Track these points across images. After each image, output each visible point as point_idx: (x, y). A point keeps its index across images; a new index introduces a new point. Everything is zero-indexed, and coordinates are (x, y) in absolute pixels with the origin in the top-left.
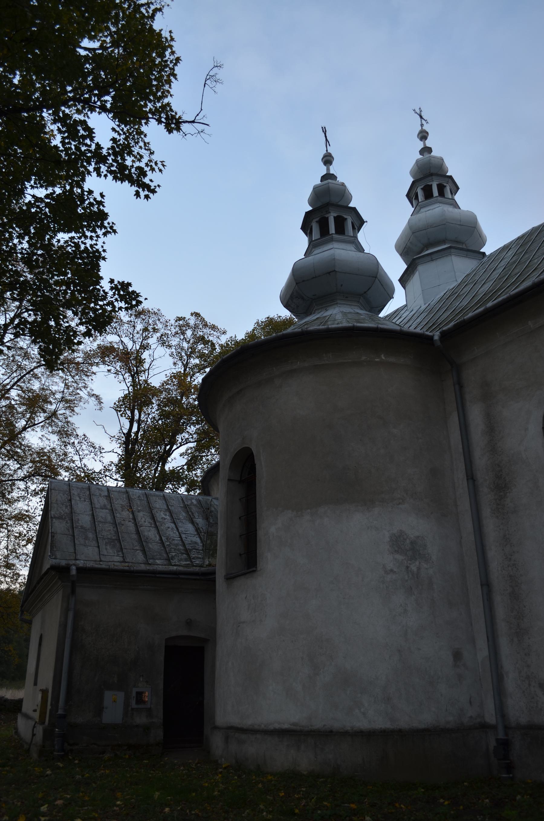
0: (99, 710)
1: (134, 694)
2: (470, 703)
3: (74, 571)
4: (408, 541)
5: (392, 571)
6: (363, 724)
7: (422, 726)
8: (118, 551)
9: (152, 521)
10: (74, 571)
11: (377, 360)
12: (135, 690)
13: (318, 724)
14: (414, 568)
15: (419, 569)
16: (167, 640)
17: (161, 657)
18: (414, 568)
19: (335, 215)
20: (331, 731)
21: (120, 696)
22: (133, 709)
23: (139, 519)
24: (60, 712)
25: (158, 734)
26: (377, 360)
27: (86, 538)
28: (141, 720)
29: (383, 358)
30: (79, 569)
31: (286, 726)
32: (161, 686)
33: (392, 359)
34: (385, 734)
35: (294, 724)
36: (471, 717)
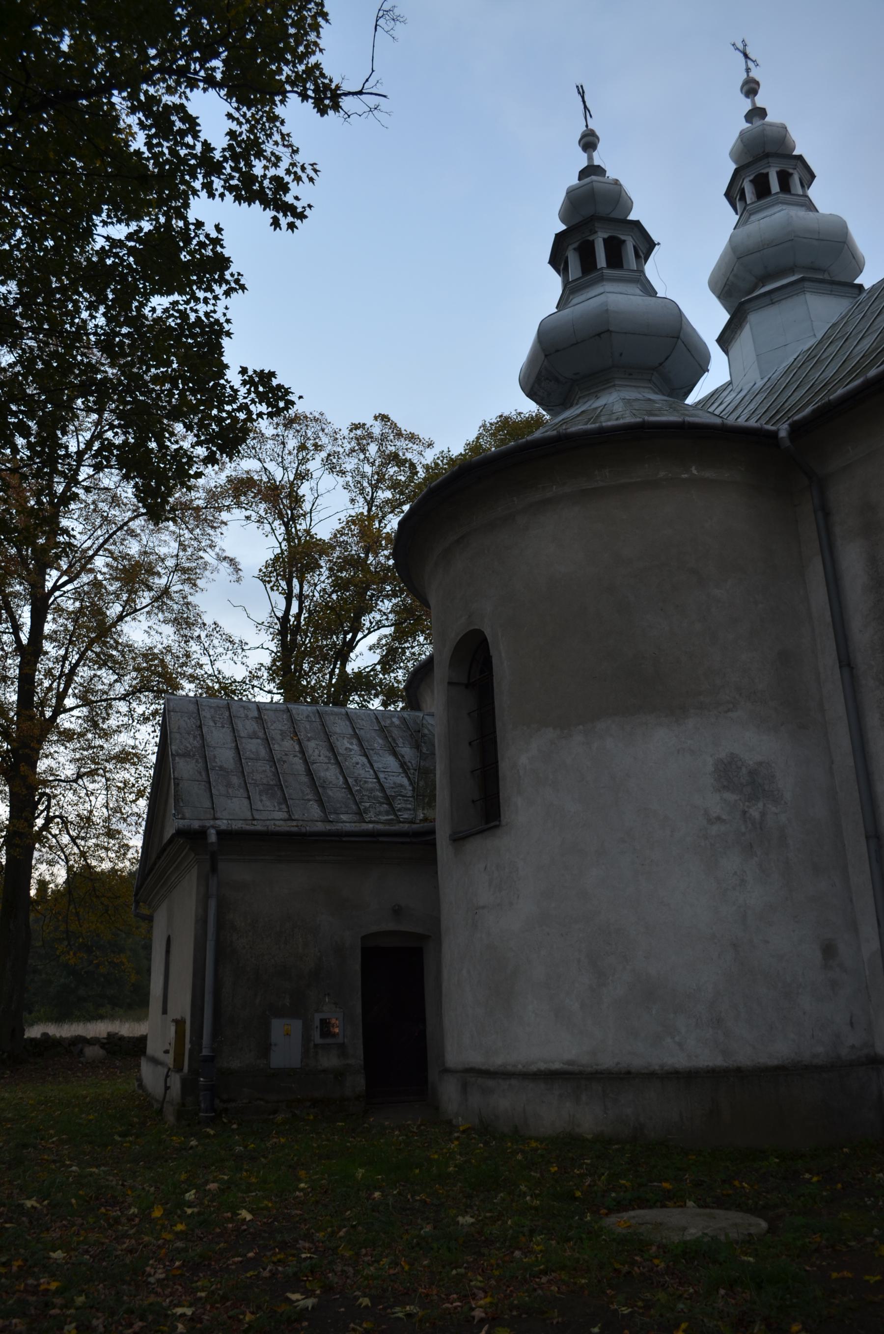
0: (265, 1048)
1: (317, 1023)
2: (852, 1024)
3: (213, 837)
4: (744, 770)
5: (718, 818)
6: (679, 1060)
7: (775, 1062)
8: (280, 804)
9: (330, 755)
10: (213, 837)
11: (685, 476)
12: (317, 1017)
13: (607, 1062)
14: (755, 813)
15: (763, 814)
16: (364, 938)
17: (355, 965)
18: (755, 813)
19: (606, 236)
20: (629, 1073)
21: (296, 1026)
22: (316, 1046)
23: (310, 752)
24: (205, 1052)
25: (357, 1083)
26: (685, 476)
27: (229, 785)
28: (330, 1061)
29: (695, 472)
30: (221, 834)
31: (557, 1066)
32: (359, 1010)
33: (709, 474)
34: (714, 1075)
35: (570, 1063)
36: (853, 1047)
